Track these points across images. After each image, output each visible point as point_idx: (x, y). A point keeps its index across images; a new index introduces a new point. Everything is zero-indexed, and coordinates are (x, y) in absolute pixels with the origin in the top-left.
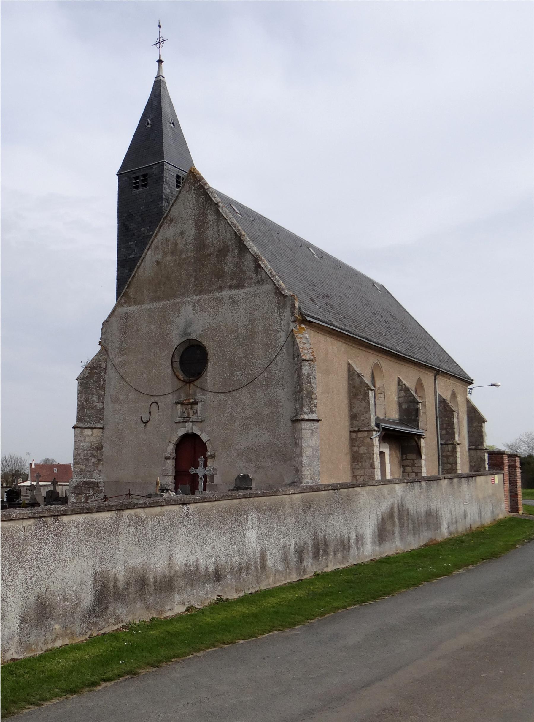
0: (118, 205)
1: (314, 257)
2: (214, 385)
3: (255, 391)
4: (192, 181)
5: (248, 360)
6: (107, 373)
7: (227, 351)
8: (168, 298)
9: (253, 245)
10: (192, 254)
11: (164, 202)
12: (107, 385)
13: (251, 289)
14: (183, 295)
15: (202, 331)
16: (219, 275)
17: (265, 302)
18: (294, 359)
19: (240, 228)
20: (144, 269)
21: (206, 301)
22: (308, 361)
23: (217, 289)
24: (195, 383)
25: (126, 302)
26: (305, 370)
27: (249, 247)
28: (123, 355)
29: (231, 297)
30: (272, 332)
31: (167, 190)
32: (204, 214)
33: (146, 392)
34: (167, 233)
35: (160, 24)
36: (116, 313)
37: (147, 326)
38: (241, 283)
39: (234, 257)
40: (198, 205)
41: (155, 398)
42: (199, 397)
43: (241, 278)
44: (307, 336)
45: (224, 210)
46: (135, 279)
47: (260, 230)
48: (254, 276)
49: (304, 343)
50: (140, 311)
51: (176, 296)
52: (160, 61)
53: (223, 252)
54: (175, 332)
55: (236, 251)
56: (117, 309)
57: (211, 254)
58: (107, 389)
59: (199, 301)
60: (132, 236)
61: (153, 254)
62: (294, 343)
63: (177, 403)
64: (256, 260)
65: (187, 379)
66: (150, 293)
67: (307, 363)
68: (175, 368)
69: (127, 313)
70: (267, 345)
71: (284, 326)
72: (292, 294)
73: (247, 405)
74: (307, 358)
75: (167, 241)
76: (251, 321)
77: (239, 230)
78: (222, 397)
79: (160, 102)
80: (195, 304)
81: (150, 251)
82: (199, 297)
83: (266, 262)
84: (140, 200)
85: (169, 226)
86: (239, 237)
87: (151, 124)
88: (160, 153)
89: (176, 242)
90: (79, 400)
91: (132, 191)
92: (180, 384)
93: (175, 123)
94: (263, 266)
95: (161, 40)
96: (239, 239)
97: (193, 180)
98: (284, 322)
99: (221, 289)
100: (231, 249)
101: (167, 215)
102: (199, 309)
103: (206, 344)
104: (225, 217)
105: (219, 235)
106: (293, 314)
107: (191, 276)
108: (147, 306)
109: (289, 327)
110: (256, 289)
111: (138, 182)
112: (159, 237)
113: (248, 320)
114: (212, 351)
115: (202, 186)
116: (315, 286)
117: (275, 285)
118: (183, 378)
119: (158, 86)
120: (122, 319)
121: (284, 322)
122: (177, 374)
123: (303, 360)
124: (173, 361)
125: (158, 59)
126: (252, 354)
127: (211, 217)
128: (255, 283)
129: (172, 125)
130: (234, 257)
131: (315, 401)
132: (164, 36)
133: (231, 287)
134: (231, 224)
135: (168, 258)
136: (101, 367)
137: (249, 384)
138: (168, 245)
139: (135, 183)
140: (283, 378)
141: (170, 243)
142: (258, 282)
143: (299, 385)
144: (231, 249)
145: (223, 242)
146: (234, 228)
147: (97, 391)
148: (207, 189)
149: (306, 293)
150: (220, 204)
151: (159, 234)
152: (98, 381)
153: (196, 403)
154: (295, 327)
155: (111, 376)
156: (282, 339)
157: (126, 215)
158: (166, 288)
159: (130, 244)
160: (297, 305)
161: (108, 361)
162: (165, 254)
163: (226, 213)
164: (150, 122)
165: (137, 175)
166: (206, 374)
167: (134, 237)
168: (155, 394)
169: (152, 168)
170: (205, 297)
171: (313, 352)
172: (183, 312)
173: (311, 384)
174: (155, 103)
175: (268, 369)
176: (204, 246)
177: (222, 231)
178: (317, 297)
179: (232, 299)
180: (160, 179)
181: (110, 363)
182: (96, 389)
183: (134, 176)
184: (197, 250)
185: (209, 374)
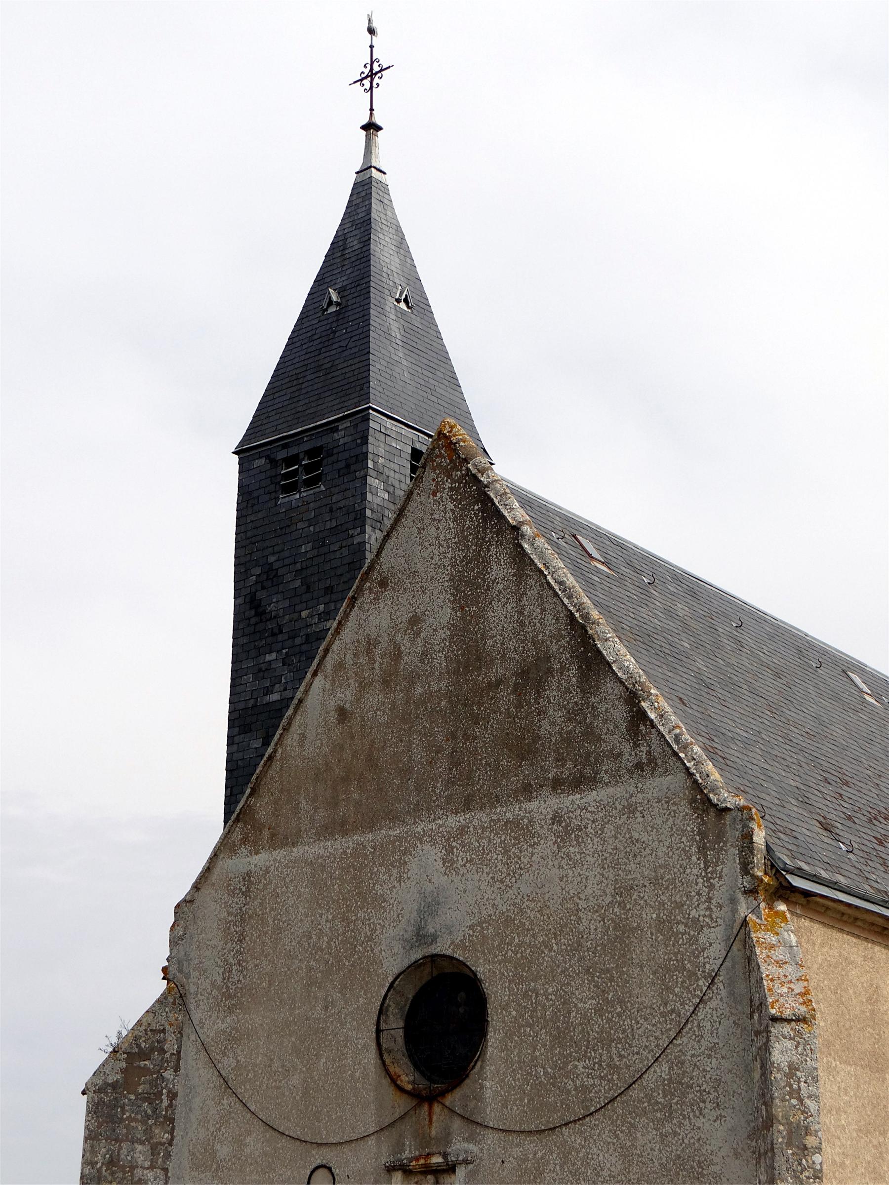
0: (237, 542)
1: (864, 701)
2: (504, 1106)
3: (633, 1126)
4: (445, 462)
5: (609, 1020)
6: (182, 1071)
7: (546, 994)
8: (370, 824)
9: (623, 651)
10: (443, 684)
11: (368, 529)
12: (180, 1113)
13: (618, 791)
14: (416, 812)
15: (471, 927)
16: (524, 748)
17: (662, 831)
18: (752, 1018)
19: (585, 600)
20: (303, 736)
21: (484, 829)
22: (789, 1021)
23: (516, 791)
24: (448, 1100)
25: (244, 840)
26: (782, 1052)
27: (610, 659)
28: (231, 1010)
29: (557, 818)
30: (681, 928)
31: (379, 495)
32: (480, 562)
33: (298, 1132)
34: (372, 619)
35: (375, 25)
36: (214, 877)
37: (306, 916)
38: (588, 771)
39: (568, 691)
40: (462, 532)
41: (324, 1150)
42: (459, 1147)
43: (589, 754)
44: (793, 939)
45: (538, 546)
46: (276, 765)
47: (670, 613)
48: (627, 747)
49: (780, 964)
50: (287, 866)
51: (393, 817)
52: (371, 127)
53: (532, 676)
54: (391, 932)
55: (574, 670)
56: (220, 863)
57: (499, 682)
58: (179, 1123)
59: (462, 830)
60: (273, 634)
61: (328, 686)
62: (750, 962)
63: (390, 1169)
64: (632, 697)
65: (423, 1084)
66: (316, 809)
67: (787, 1029)
68: (390, 1052)
69: (249, 874)
70: (669, 970)
71: (720, 906)
72: (743, 802)
73: (605, 1173)
74: (787, 1013)
75: (371, 644)
76: (617, 892)
77: (580, 607)
78: (530, 1145)
79: (366, 242)
80: (449, 843)
81: (319, 681)
82: (462, 819)
83: (662, 703)
84: (300, 525)
85: (377, 599)
86: (583, 627)
87: (338, 304)
88: (359, 384)
89: (397, 647)
90: (88, 1162)
91: (277, 498)
92: (403, 1104)
93: (416, 302)
94: (652, 716)
95: (376, 68)
96: (580, 633)
97: (451, 462)
98: (720, 895)
99: (527, 791)
100: (557, 666)
101: (371, 568)
102: (462, 857)
103: (481, 970)
104: (541, 566)
105: (522, 624)
106: (746, 868)
107: (437, 752)
108: (310, 850)
109: (735, 911)
110: (632, 789)
111: (295, 473)
112: (348, 634)
113: (610, 890)
114: (498, 993)
115: (474, 476)
116: (846, 783)
117: (690, 775)
118: (413, 1083)
119: (365, 195)
120: (232, 894)
121: (720, 895)
122: (393, 1069)
123: (775, 1019)
124: (383, 1026)
125: (365, 121)
126: (621, 1002)
127: (500, 569)
128: (630, 772)
129: (403, 305)
130: (568, 691)
131: (817, 1158)
132: (383, 57)
133: (557, 785)
134: (556, 587)
135: (374, 699)
136: (162, 1051)
137: (613, 1100)
138: (372, 661)
139: (287, 476)
140: (718, 1082)
141: (378, 653)
142: (639, 766)
143: (765, 1103)
144: (557, 666)
145: (535, 643)
146: (566, 601)
147: (148, 1131)
148: (487, 486)
149: (805, 802)
150: (526, 529)
151: (349, 624)
152: (153, 1098)
153: (451, 1169)
154: (755, 910)
155: (194, 1081)
156: (716, 951)
157: (258, 571)
158: (370, 792)
159: (268, 658)
160: (759, 837)
161: (187, 1030)
162: (363, 686)
163: (542, 556)
164: (335, 298)
165: (293, 451)
166: (482, 1068)
167: (280, 637)
168: (324, 1137)
169: (336, 430)
170: (482, 817)
171: (806, 992)
172: (413, 867)
173: (801, 1101)
174: (354, 244)
175: (673, 1051)
176: (479, 659)
177: (532, 609)
178: (849, 818)
179: (560, 822)
180: (355, 462)
181: (193, 1037)
182: (144, 1122)
183: (281, 455)
184: (456, 672)
185: (489, 1069)
